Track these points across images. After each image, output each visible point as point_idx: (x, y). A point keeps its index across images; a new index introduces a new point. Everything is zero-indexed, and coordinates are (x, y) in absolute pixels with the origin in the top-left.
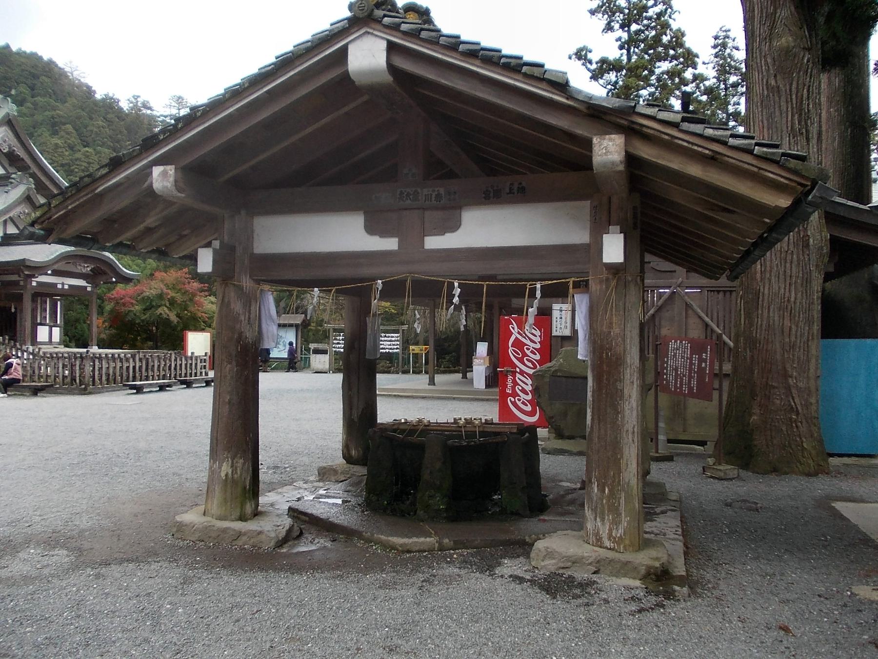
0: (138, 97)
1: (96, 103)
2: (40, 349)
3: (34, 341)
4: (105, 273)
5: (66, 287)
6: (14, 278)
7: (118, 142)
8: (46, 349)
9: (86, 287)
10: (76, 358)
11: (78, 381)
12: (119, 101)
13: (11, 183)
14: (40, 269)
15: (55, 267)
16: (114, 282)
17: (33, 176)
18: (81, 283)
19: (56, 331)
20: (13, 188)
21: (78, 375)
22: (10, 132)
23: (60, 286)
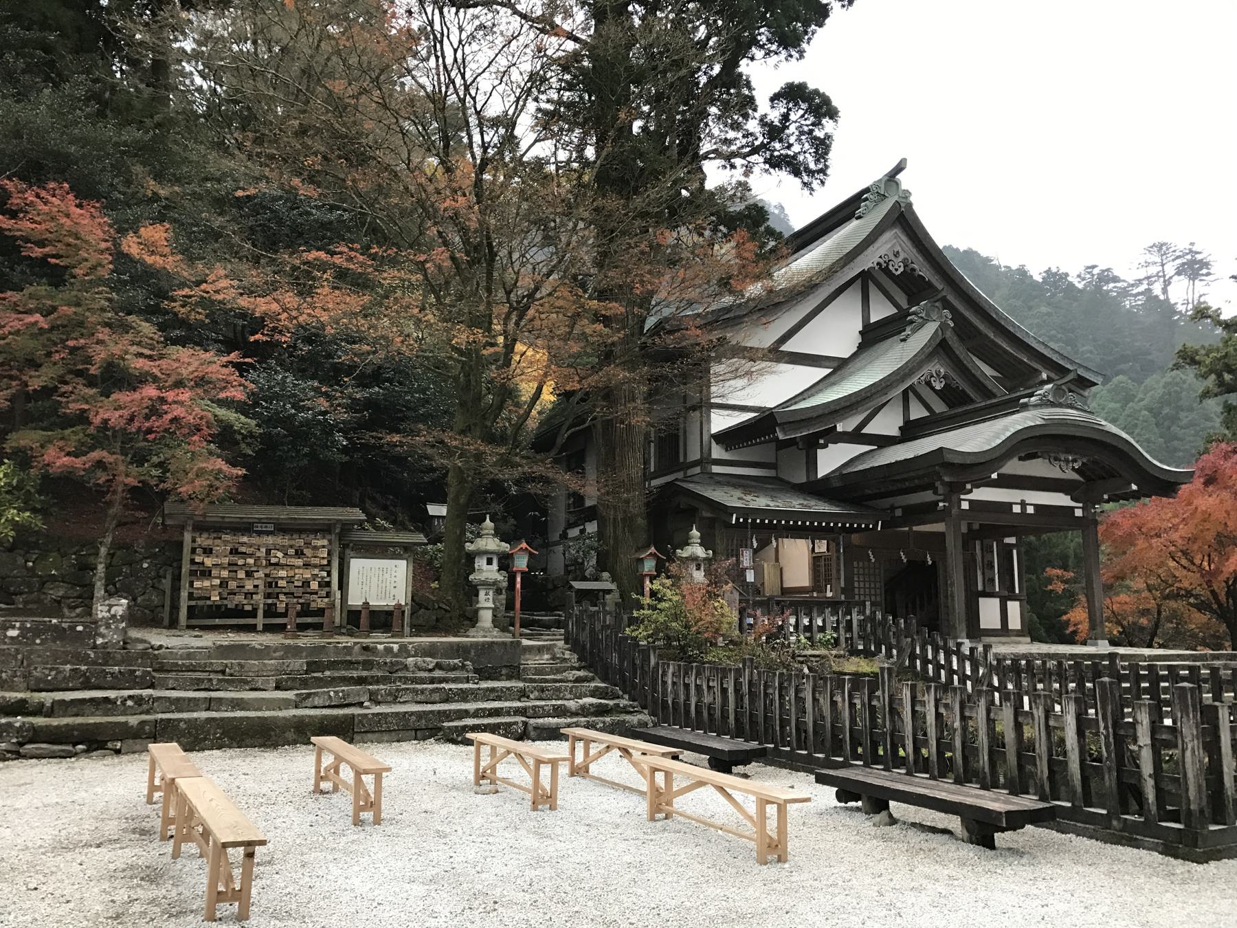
0: (1094, 267)
2: (987, 648)
3: (975, 632)
4: (1111, 474)
5: (1030, 510)
8: (1003, 648)
9: (1073, 508)
11: (1151, 795)
12: (1067, 275)
13: (912, 322)
14: (977, 469)
17: (946, 304)
19: (1014, 608)
20: (914, 331)
21: (1147, 768)
22: (904, 238)
23: (1017, 509)
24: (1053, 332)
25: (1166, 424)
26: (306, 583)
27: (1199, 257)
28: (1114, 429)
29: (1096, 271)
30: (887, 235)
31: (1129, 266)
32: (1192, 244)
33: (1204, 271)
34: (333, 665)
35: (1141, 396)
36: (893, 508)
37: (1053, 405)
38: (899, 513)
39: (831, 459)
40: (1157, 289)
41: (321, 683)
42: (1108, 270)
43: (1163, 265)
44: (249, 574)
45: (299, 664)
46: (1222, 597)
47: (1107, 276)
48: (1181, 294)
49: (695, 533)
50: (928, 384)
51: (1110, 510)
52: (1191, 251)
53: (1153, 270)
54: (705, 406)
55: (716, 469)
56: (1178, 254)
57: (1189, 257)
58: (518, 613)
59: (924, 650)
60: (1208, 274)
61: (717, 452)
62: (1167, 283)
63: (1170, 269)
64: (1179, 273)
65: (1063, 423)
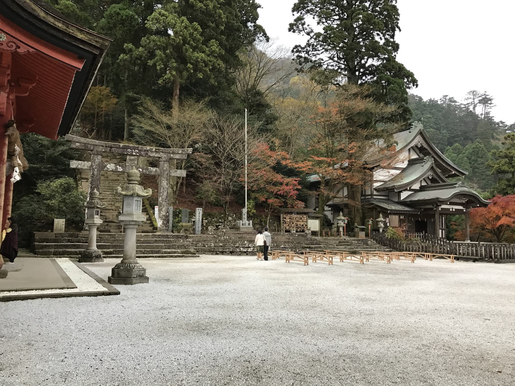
0: (447, 96)
1: (425, 105)
4: (473, 202)
5: (454, 210)
6: (431, 206)
7: (439, 124)
10: (469, 246)
14: (444, 202)
15: (452, 201)
16: (478, 207)
17: (433, 157)
18: (461, 207)
24: (432, 125)
25: (473, 163)
26: (303, 225)
27: (488, 97)
28: (475, 192)
29: (448, 98)
30: (418, 137)
31: (461, 99)
32: (485, 92)
33: (489, 102)
34: (343, 242)
35: (464, 151)
36: (421, 208)
37: (461, 187)
38: (423, 210)
39: (404, 195)
40: (471, 108)
41: (340, 245)
42: (452, 98)
43: (474, 99)
44: (293, 223)
45: (338, 242)
46: (496, 230)
47: (451, 100)
48: (479, 110)
49: (381, 215)
50: (428, 177)
51: (471, 209)
52: (485, 94)
53: (470, 101)
54: (372, 181)
55: (375, 197)
56: (480, 95)
57: (484, 97)
58: (345, 233)
59: (438, 241)
60: (490, 104)
61: (375, 193)
62: (475, 106)
63: (476, 101)
64: (479, 103)
65: (464, 191)
